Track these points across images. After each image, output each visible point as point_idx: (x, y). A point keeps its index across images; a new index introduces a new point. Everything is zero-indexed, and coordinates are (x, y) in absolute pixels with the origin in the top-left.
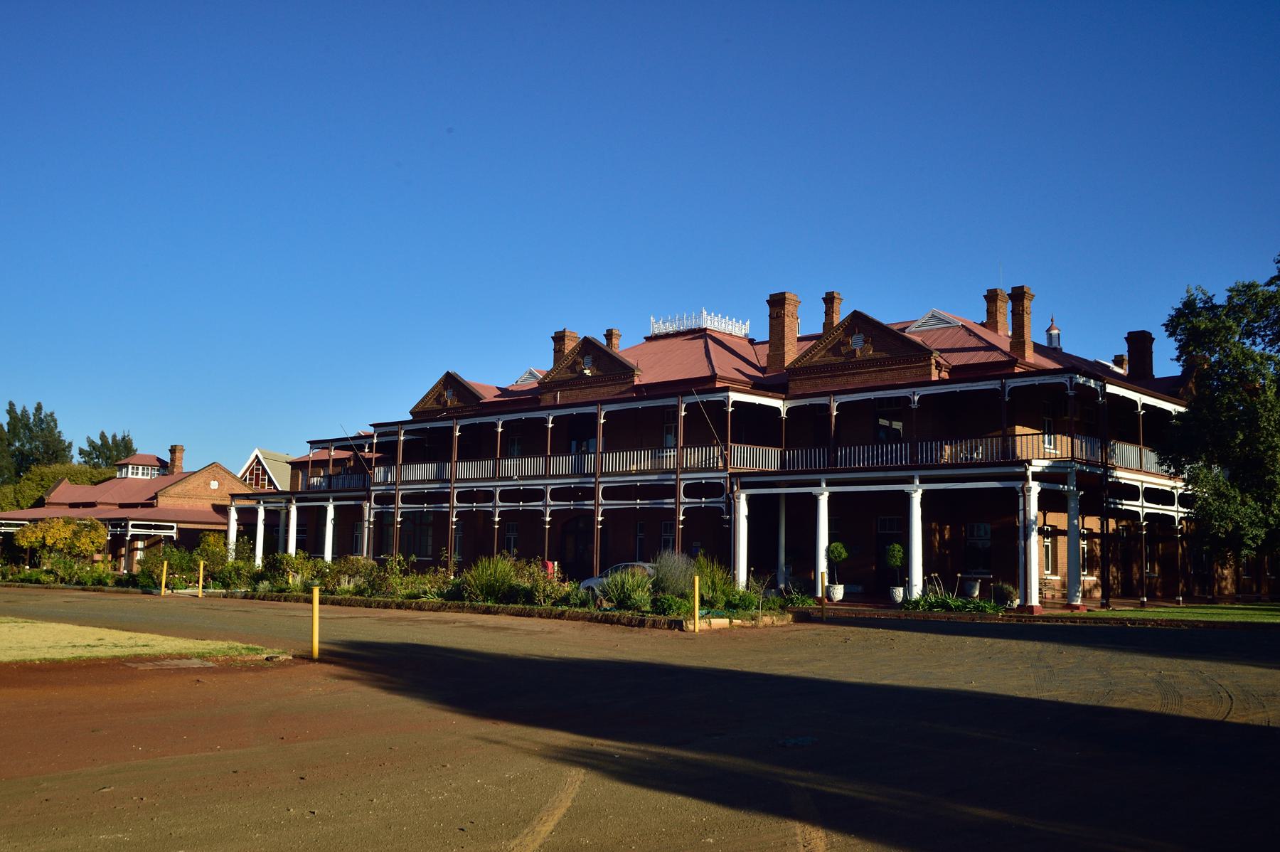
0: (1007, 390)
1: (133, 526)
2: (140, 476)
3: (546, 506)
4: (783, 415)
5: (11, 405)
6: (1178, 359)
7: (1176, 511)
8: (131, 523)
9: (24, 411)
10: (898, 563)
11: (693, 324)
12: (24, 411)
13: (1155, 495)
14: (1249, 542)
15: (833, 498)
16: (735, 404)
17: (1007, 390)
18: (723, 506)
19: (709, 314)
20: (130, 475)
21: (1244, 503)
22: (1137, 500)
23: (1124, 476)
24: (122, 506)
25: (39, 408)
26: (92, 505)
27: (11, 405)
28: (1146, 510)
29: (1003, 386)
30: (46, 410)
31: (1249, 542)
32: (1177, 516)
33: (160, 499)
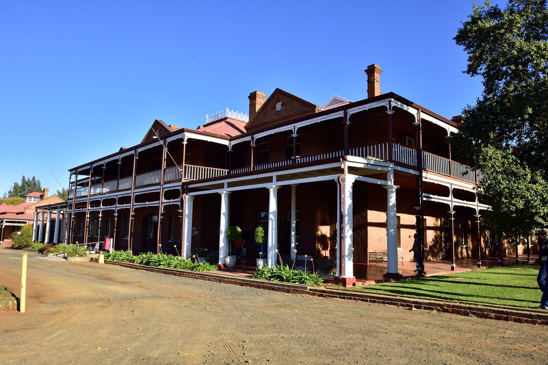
0: (348, 116)
1: (6, 222)
2: (32, 201)
3: (116, 207)
4: (230, 149)
5: (24, 177)
6: (472, 70)
7: (477, 206)
8: (5, 220)
9: (29, 180)
10: (261, 241)
11: (220, 117)
12: (29, 180)
13: (459, 194)
14: (540, 220)
15: (232, 196)
16: (189, 140)
17: (348, 116)
18: (179, 203)
19: (230, 110)
20: (27, 201)
21: (534, 182)
22: (448, 196)
23: (429, 177)
24: (18, 214)
25: (34, 178)
26: (5, 213)
27: (24, 177)
28: (455, 204)
29: (346, 114)
30: (37, 179)
31: (540, 220)
32: (478, 209)
33: (27, 210)
